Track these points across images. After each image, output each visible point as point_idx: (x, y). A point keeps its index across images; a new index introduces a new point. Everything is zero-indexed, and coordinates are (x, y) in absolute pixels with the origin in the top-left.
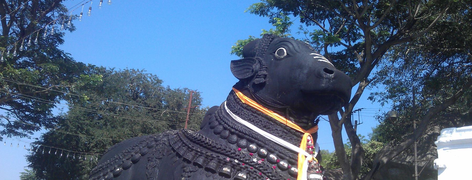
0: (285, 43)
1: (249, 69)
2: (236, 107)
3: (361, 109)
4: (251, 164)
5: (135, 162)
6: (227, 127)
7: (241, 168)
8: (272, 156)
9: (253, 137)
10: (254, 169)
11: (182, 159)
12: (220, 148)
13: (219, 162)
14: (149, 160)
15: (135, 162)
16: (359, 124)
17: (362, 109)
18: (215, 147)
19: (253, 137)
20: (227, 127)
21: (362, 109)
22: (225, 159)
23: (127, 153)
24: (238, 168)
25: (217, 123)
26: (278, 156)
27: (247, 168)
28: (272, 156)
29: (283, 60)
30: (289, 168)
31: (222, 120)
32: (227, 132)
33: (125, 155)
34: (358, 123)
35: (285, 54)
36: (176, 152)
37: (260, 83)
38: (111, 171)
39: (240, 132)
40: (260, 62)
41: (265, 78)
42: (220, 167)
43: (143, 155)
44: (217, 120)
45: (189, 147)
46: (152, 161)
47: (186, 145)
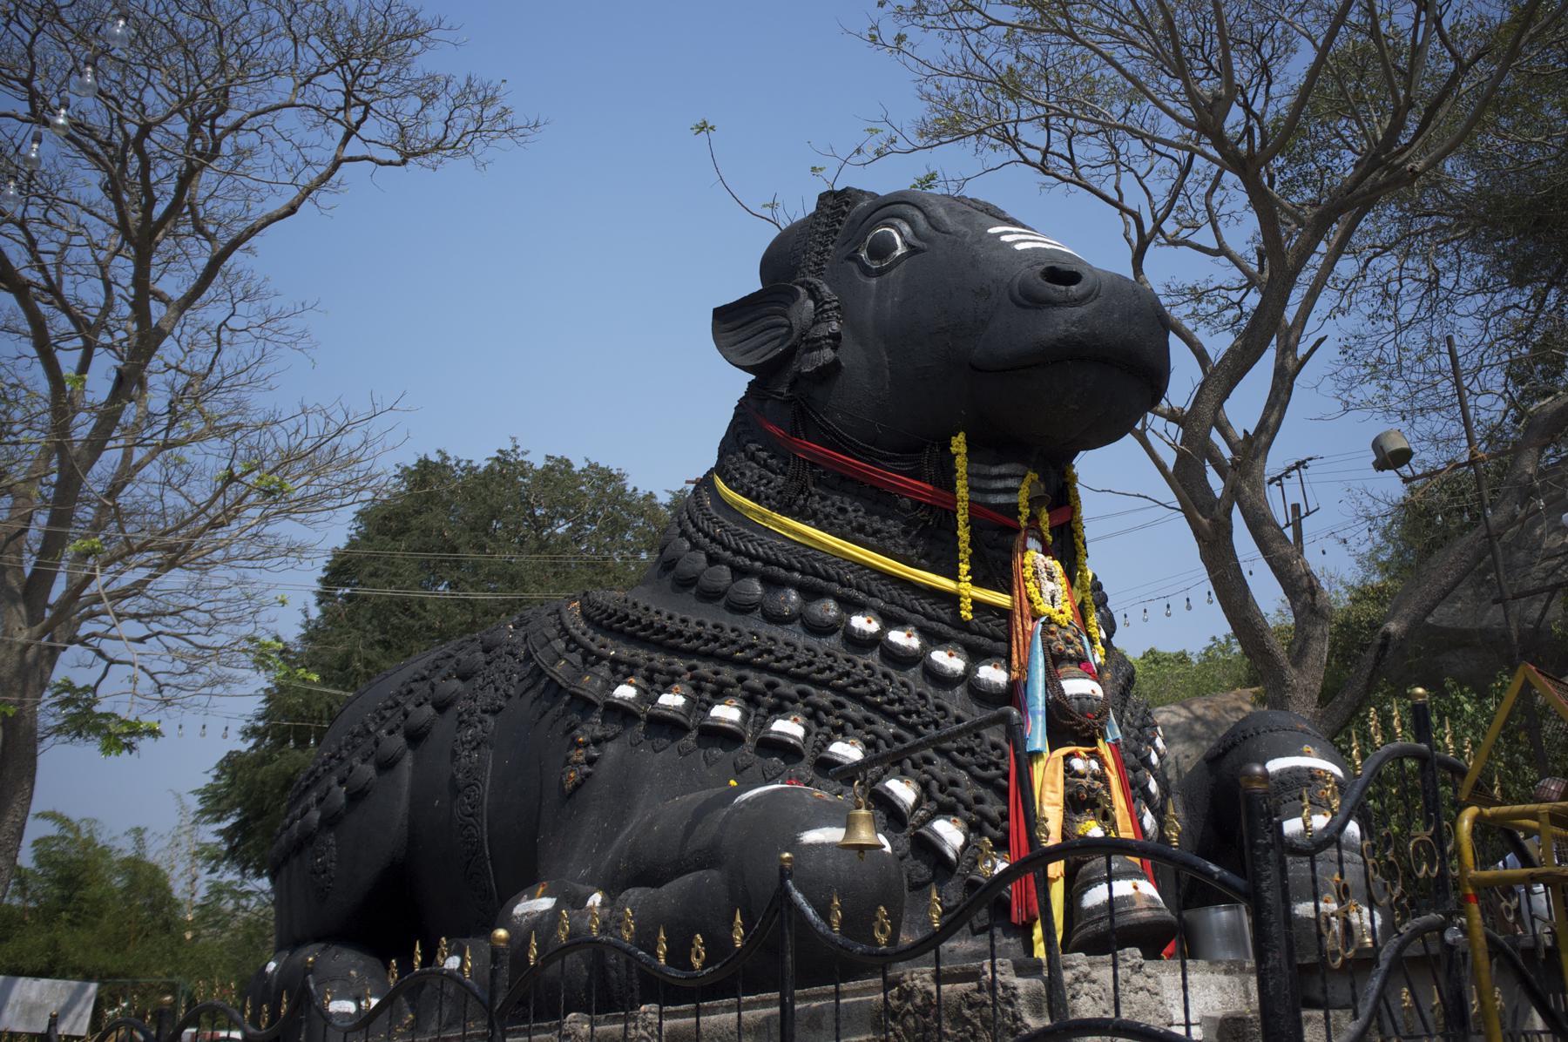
0: (897, 222)
1: (780, 326)
2: (748, 473)
3: (1304, 462)
4: (819, 676)
5: (416, 737)
6: (721, 551)
7: (783, 698)
8: (897, 637)
9: (817, 574)
10: (864, 712)
11: (641, 726)
12: (698, 636)
13: (698, 689)
14: (461, 723)
15: (416, 737)
16: (1307, 514)
17: (1310, 459)
18: (680, 634)
19: (817, 574)
20: (721, 551)
21: (1310, 459)
22: (716, 673)
23: (392, 708)
24: (769, 699)
25: (687, 545)
26: (923, 632)
27: (803, 694)
28: (939, 657)
29: (893, 272)
30: (970, 671)
31: (699, 530)
32: (725, 571)
33: (383, 718)
34: (1303, 511)
35: (901, 250)
36: (1185, 914)
37: (818, 368)
38: (341, 782)
39: (767, 562)
40: (813, 292)
41: (835, 348)
42: (704, 705)
43: (442, 707)
44: (684, 534)
45: (588, 652)
46: (470, 725)
47: (580, 645)
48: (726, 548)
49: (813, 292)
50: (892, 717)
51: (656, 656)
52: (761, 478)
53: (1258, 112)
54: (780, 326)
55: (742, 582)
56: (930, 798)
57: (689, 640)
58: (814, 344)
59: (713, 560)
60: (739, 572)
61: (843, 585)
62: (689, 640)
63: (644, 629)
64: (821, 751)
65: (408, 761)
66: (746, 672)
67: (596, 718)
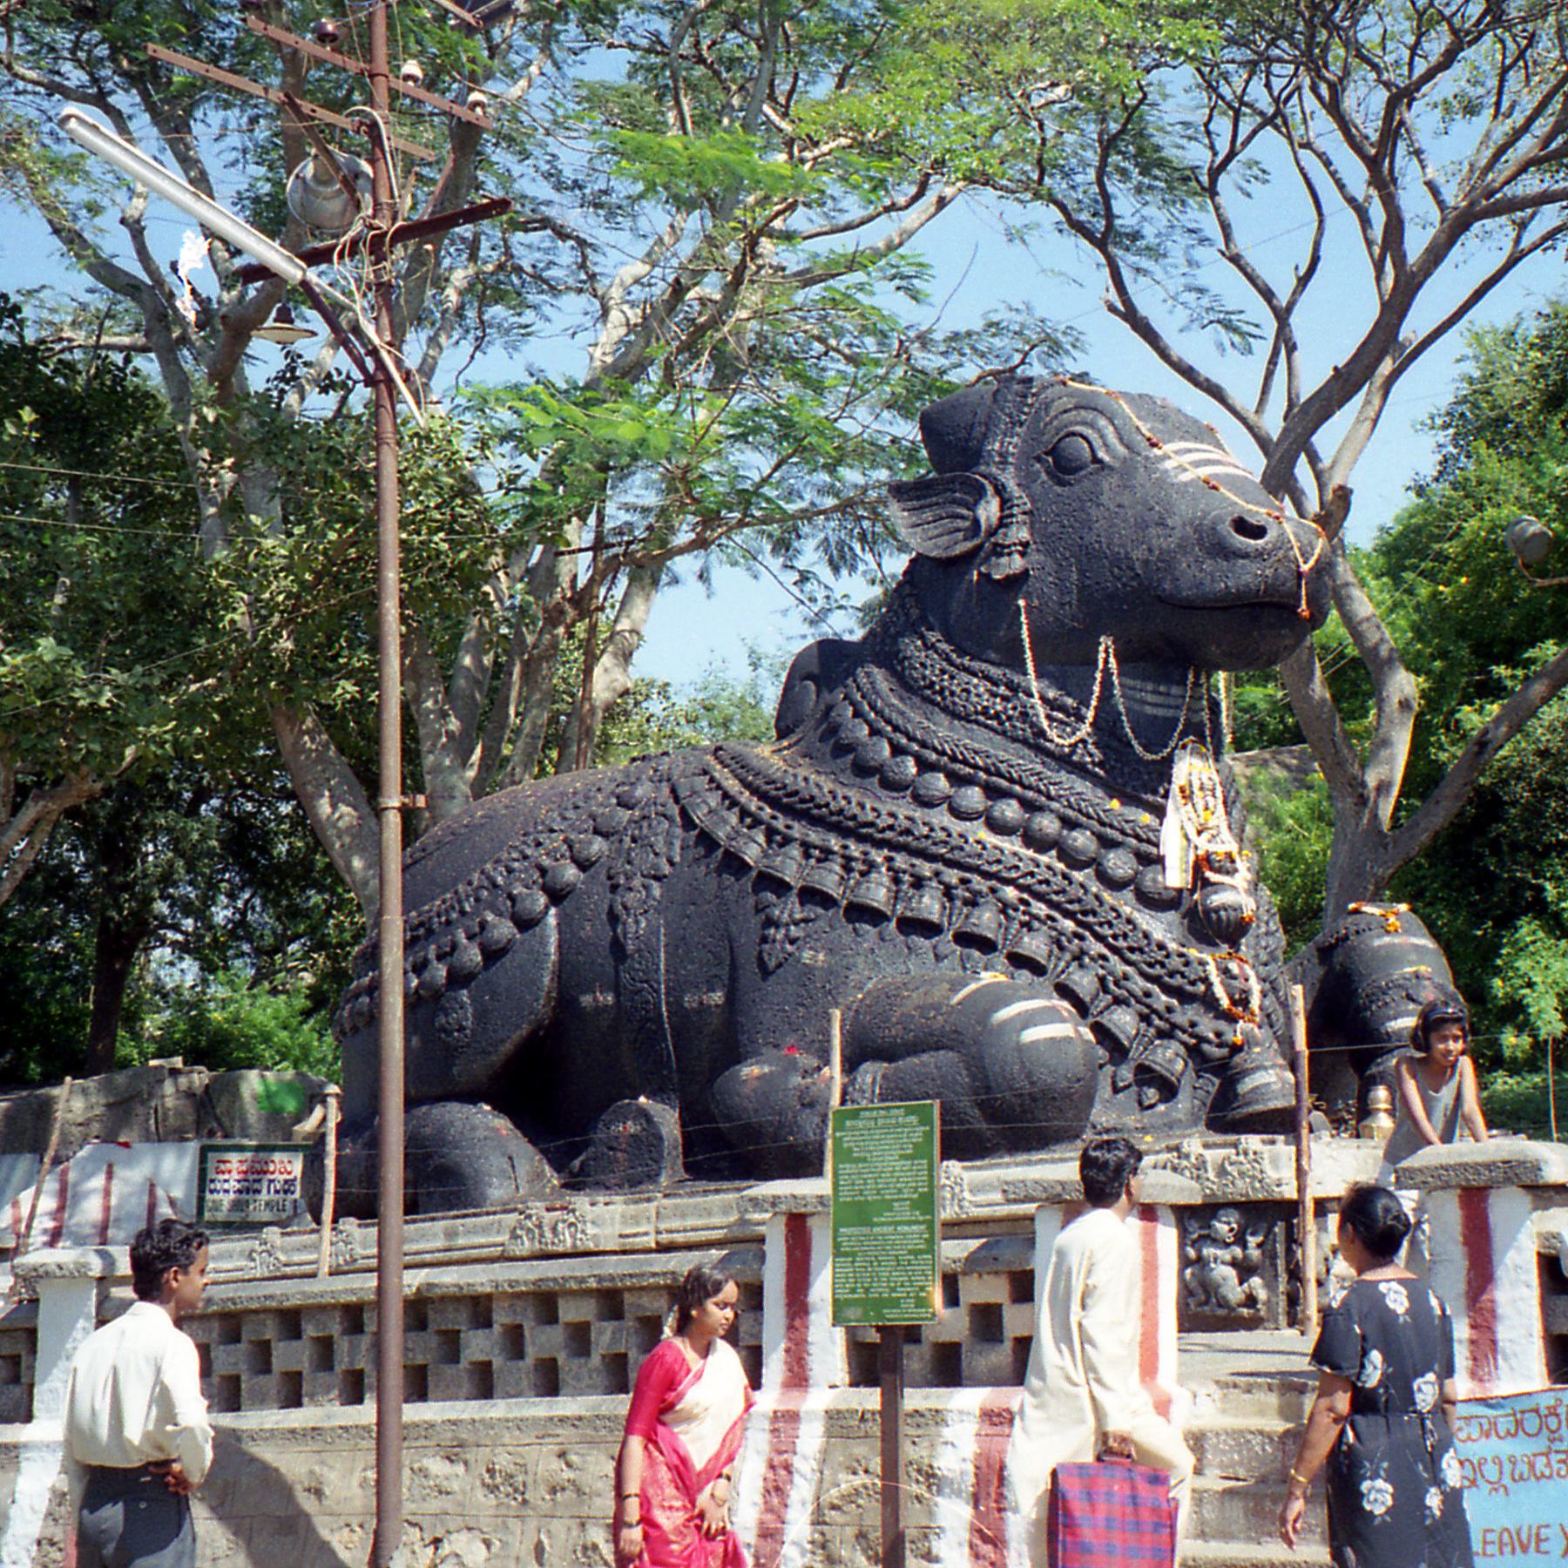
18: (871, 824)
19: (1000, 775)
25: (850, 711)
48: (889, 722)
49: (1000, 490)
50: (1100, 938)
51: (796, 825)
52: (943, 672)
53: (699, 1462)
54: (963, 517)
55: (927, 776)
56: (1106, 990)
57: (882, 831)
58: (999, 550)
59: (897, 750)
60: (924, 766)
61: (1024, 787)
62: (882, 831)
63: (789, 795)
64: (1464, 737)
65: (552, 920)
66: (917, 862)
67: (793, 898)
